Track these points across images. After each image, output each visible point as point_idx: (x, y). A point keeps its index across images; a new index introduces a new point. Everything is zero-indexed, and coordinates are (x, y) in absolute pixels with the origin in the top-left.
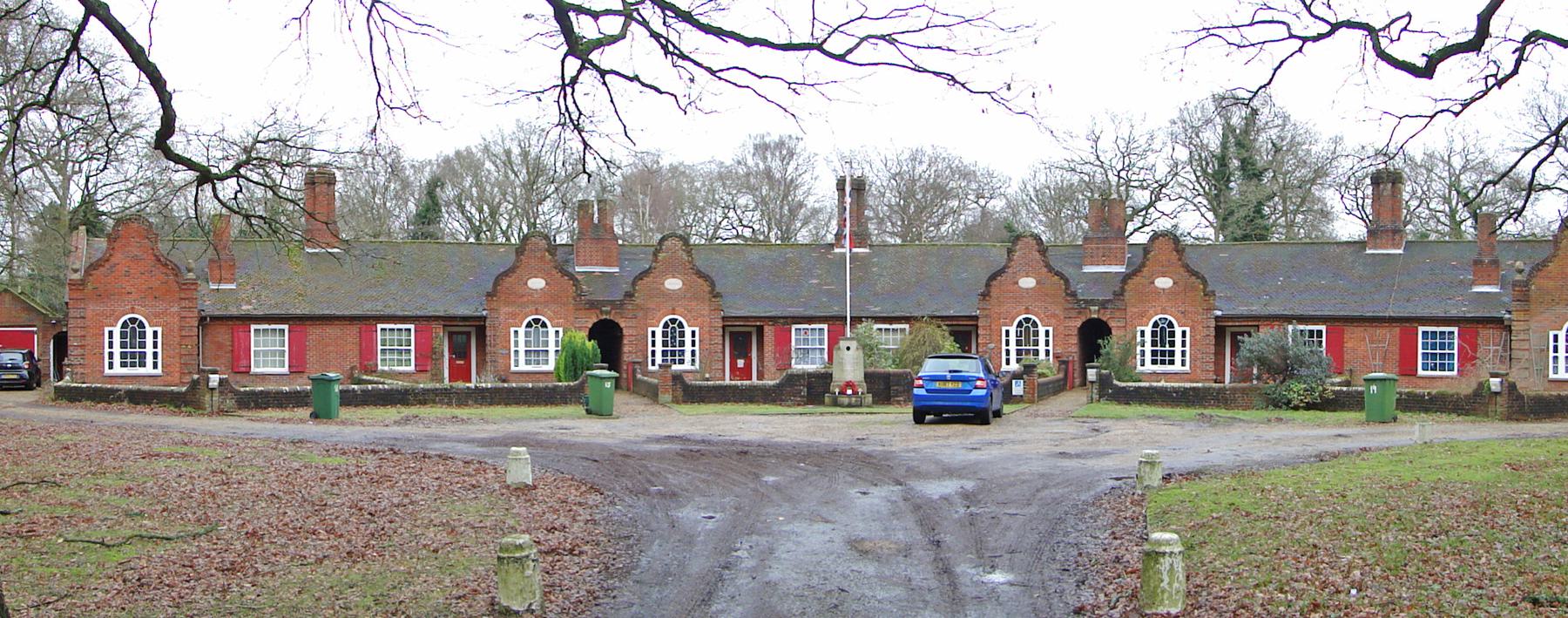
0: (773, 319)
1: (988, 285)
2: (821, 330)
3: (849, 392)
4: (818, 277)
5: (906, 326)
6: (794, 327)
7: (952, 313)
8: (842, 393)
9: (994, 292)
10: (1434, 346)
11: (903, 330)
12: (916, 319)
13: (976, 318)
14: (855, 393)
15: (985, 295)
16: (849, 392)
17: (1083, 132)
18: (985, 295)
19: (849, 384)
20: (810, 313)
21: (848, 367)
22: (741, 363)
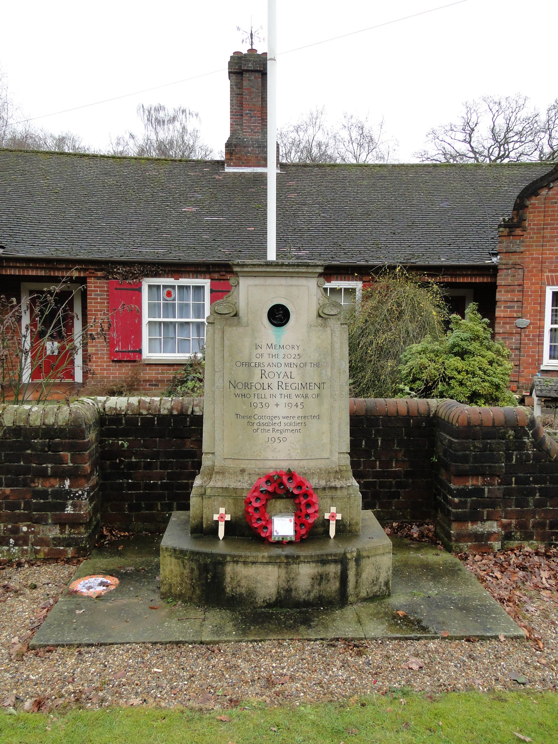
0: (104, 267)
1: (520, 205)
2: (199, 289)
3: (283, 526)
4: (197, 203)
5: (358, 285)
6: (146, 283)
7: (443, 261)
8: (248, 531)
9: (532, 218)
10: (169, 309)
11: (350, 292)
12: (378, 270)
13: (493, 270)
14: (311, 532)
15: (514, 225)
16: (283, 526)
17: (460, 123)
18: (514, 225)
19: (284, 488)
20: (175, 256)
21: (279, 407)
22: (51, 347)
